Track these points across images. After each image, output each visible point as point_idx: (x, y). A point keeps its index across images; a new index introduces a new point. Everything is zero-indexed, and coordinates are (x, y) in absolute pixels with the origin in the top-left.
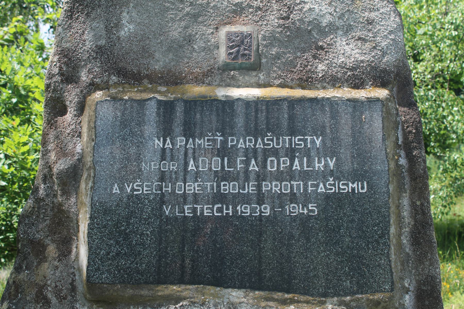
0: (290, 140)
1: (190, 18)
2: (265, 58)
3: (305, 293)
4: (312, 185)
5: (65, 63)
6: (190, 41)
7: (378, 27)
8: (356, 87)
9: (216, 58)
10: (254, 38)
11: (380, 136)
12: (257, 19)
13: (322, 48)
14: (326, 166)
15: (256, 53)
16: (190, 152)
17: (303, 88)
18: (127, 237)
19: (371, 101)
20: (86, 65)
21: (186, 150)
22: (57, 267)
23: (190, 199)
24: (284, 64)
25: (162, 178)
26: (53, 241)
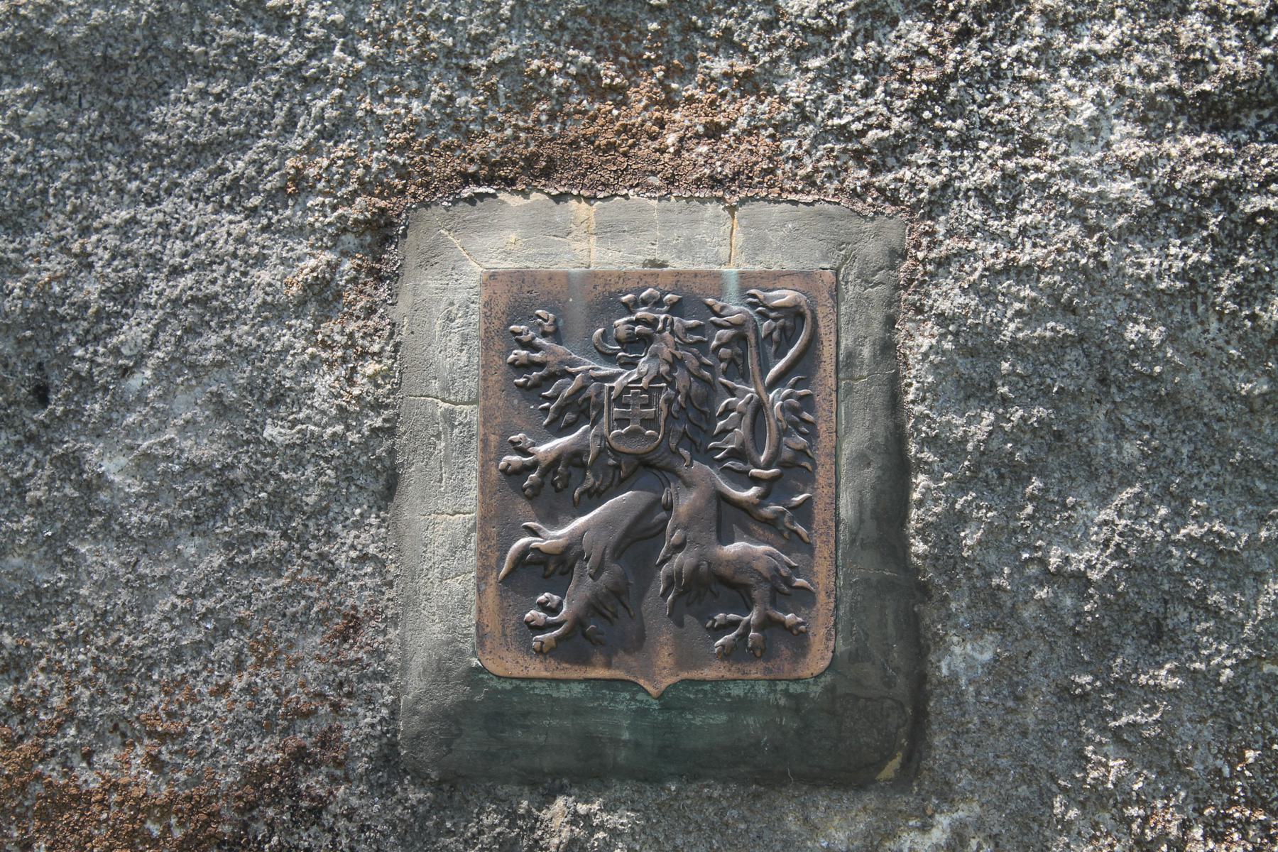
1: (53, 93)
2: (977, 630)
6: (41, 395)
9: (354, 624)
10: (847, 363)
15: (869, 566)
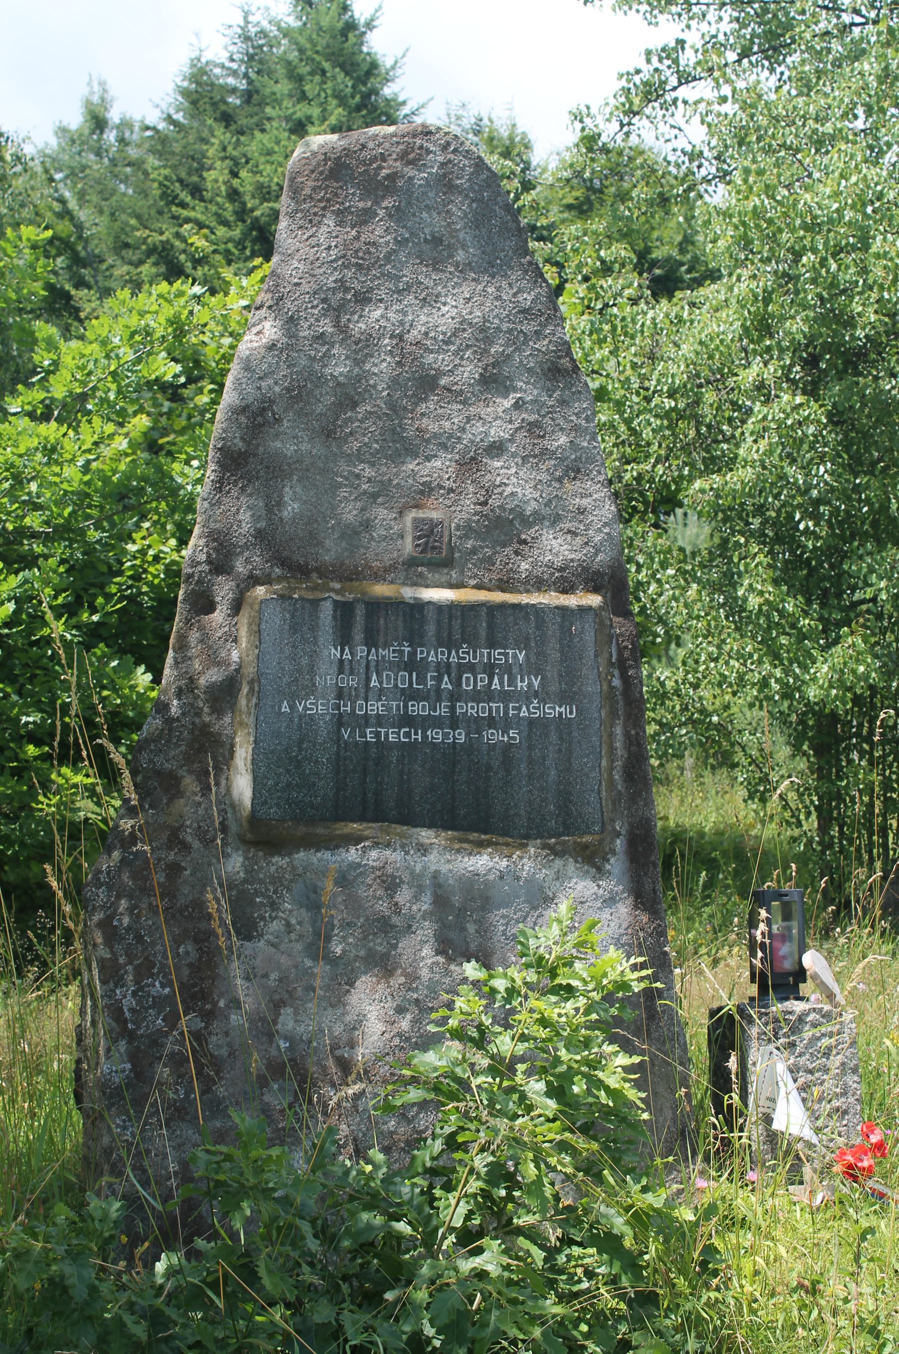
0: (489, 654)
3: (505, 834)
4: (514, 708)
5: (214, 549)
7: (591, 518)
8: (565, 591)
11: (592, 654)
12: (448, 503)
13: (525, 542)
14: (530, 685)
16: (373, 664)
17: (503, 591)
18: (299, 764)
19: (583, 610)
20: (242, 553)
21: (368, 662)
22: (199, 804)
23: (373, 721)
24: (481, 561)
25: (340, 695)
26: (190, 772)
